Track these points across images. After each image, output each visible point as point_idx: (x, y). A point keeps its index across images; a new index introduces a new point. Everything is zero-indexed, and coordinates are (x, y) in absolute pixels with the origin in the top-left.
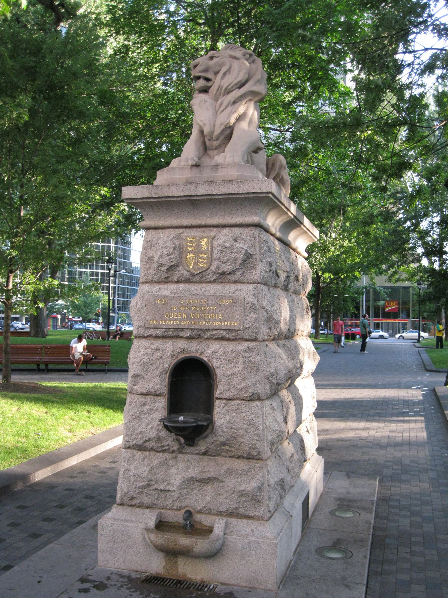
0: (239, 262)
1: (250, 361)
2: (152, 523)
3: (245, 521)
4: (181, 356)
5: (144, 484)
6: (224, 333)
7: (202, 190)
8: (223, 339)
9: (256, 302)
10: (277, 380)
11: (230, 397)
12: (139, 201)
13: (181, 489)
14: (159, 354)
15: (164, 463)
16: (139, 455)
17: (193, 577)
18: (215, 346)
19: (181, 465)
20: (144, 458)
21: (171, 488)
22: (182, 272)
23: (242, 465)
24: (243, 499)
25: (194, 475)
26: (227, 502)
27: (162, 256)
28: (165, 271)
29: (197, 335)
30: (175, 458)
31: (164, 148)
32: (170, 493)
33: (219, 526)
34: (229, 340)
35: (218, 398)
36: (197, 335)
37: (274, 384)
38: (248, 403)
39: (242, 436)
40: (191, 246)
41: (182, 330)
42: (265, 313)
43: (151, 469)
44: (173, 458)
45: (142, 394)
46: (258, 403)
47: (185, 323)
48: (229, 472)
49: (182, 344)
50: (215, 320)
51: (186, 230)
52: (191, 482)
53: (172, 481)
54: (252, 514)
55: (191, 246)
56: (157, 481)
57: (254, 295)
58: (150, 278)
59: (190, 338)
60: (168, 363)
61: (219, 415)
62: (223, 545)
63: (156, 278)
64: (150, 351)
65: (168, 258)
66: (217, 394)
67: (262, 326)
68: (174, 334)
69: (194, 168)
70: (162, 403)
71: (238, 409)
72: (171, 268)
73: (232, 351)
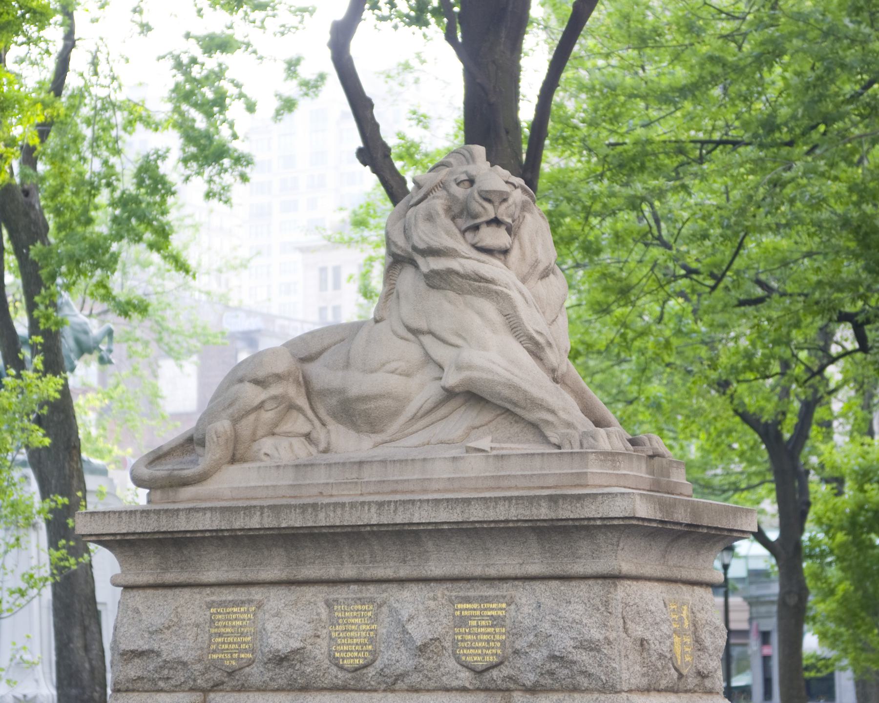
63: (645, 681)
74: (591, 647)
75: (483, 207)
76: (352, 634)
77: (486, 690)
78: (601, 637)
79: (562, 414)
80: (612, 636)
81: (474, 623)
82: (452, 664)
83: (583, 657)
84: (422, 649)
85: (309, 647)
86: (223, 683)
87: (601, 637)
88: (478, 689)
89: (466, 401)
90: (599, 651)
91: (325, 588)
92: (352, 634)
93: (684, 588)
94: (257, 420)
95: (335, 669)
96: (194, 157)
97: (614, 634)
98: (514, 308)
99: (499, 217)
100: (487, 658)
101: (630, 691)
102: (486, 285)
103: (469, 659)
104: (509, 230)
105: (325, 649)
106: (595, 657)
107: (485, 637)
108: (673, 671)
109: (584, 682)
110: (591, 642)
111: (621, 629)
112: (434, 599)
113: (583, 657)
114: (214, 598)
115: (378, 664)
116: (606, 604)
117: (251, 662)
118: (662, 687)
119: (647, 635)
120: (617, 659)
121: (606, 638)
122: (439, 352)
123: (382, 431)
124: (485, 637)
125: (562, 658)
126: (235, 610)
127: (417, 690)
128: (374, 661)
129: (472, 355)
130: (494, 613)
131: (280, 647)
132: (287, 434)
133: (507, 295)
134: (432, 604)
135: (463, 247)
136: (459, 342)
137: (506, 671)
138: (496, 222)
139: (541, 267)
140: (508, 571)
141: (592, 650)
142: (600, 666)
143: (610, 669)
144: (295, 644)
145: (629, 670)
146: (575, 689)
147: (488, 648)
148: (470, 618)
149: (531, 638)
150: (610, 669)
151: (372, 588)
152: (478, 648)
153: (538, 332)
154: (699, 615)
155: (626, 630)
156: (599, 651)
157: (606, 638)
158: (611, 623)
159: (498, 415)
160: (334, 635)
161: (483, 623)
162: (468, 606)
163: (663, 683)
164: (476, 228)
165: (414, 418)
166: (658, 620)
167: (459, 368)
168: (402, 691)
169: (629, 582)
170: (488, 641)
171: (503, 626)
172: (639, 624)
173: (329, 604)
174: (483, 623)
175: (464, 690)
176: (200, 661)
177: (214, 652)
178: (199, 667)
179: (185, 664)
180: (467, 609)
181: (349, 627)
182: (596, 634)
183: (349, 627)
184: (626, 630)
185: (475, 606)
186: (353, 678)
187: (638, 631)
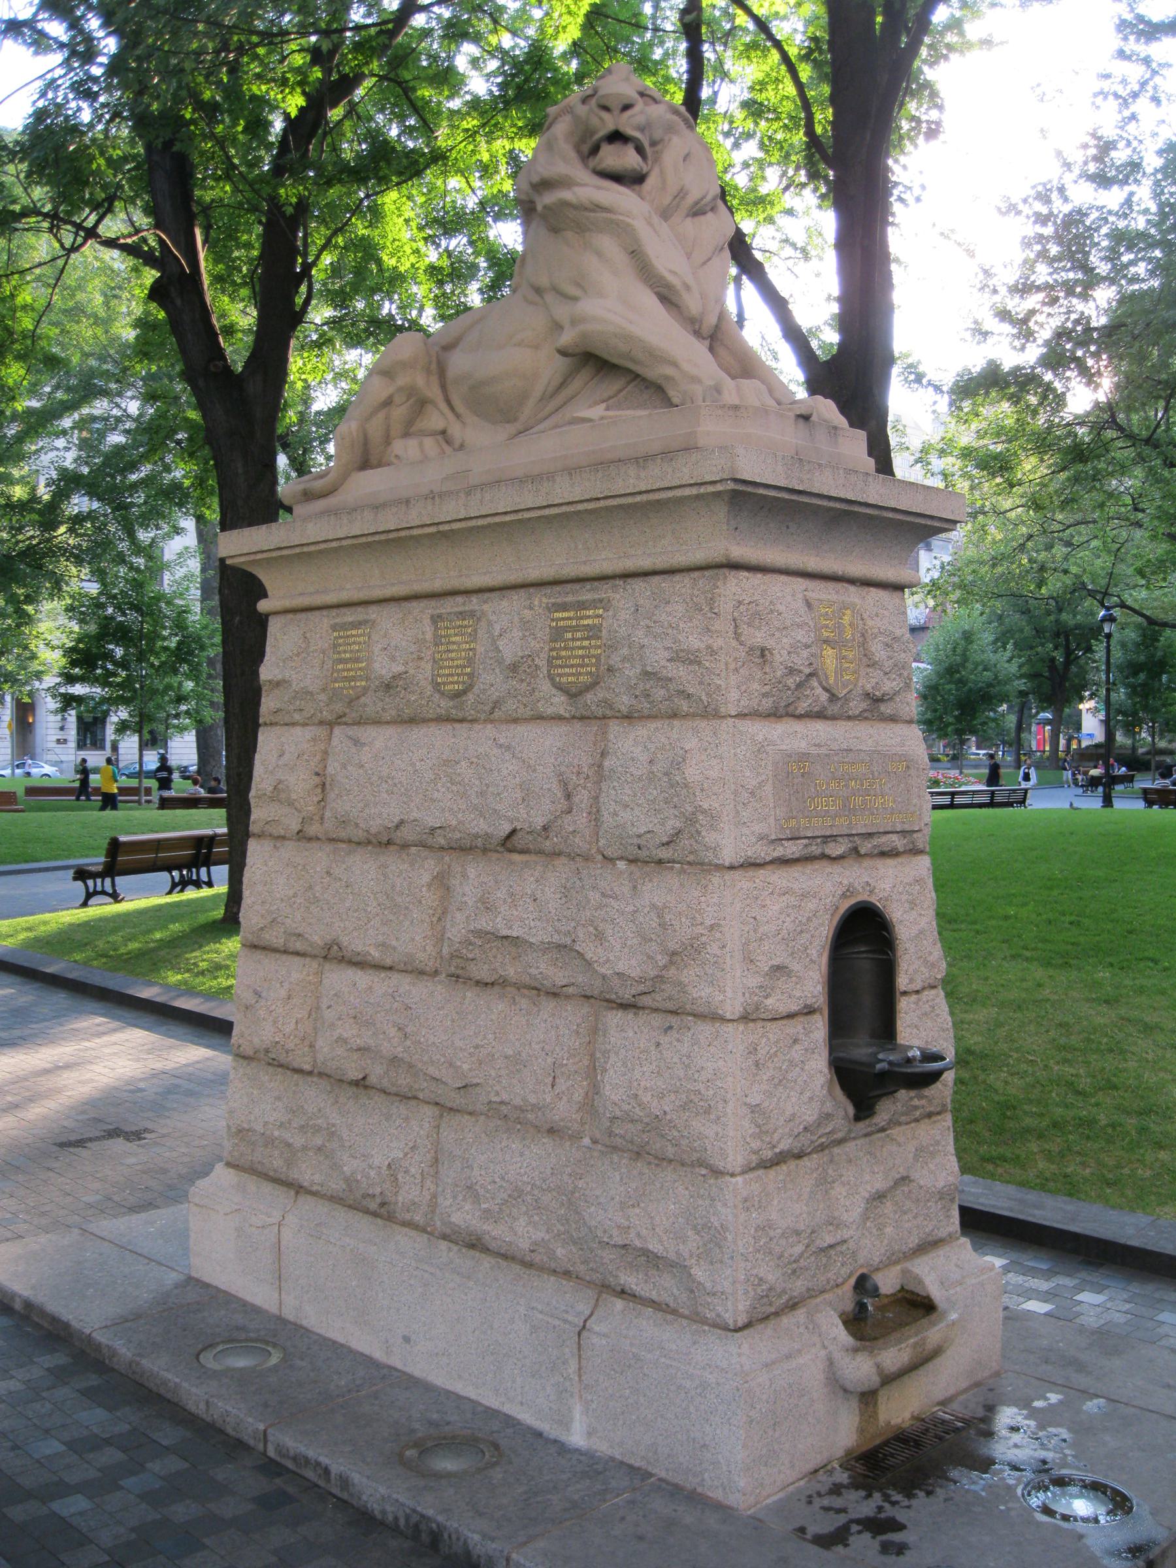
4: (846, 905)
12: (761, 491)
16: (774, 1176)
17: (899, 1420)
21: (846, 1233)
27: (793, 650)
28: (793, 686)
32: (839, 1248)
35: (905, 993)
41: (832, 838)
45: (791, 1016)
47: (841, 825)
53: (845, 1217)
58: (754, 704)
61: (908, 1030)
63: (767, 704)
64: (793, 900)
66: (902, 982)
69: (801, 421)
70: (819, 1029)
74: (690, 659)
75: (601, 119)
76: (453, 655)
77: (582, 718)
78: (703, 646)
79: (685, 366)
80: (718, 643)
81: (569, 635)
82: (545, 687)
83: (680, 672)
84: (514, 668)
85: (412, 671)
86: (345, 715)
87: (703, 646)
88: (574, 717)
89: (598, 371)
90: (699, 663)
91: (433, 603)
92: (453, 655)
93: (852, 588)
94: (387, 418)
95: (437, 696)
96: (1159, 518)
97: (720, 642)
98: (636, 240)
99: (622, 129)
100: (581, 679)
101: (741, 716)
102: (609, 215)
103: (564, 680)
104: (640, 150)
105: (429, 674)
106: (695, 672)
107: (580, 652)
108: (819, 691)
109: (685, 706)
110: (688, 652)
111: (731, 634)
112: (531, 608)
113: (680, 672)
114: (338, 620)
115: (476, 690)
116: (711, 601)
117: (365, 690)
118: (800, 711)
119: (770, 643)
120: (723, 674)
121: (709, 647)
122: (562, 312)
123: (516, 420)
124: (580, 652)
125: (654, 674)
126: (354, 632)
127: (515, 721)
128: (471, 686)
129: (590, 307)
130: (589, 621)
131: (384, 672)
132: (423, 433)
133: (628, 225)
134: (527, 613)
135: (580, 173)
136: (572, 290)
137: (601, 694)
138: (616, 137)
139: (690, 200)
140: (608, 568)
141: (691, 662)
142: (701, 683)
143: (713, 688)
144: (398, 668)
145: (736, 688)
146: (674, 715)
147: (582, 666)
148: (566, 629)
149: (625, 651)
150: (713, 688)
151: (474, 599)
152: (572, 666)
153: (671, 271)
154: (870, 623)
155: (737, 636)
156: (699, 663)
157: (709, 647)
158: (717, 627)
159: (629, 383)
160: (437, 656)
161: (579, 635)
162: (565, 615)
163: (803, 706)
164: (595, 150)
165: (545, 398)
166: (788, 623)
167: (574, 322)
168: (501, 721)
169: (746, 574)
170: (582, 657)
171: (599, 638)
172: (759, 628)
173: (436, 619)
174: (579, 635)
175: (559, 718)
176: (323, 690)
177: (336, 681)
178: (323, 697)
179: (311, 693)
180: (563, 619)
181: (451, 647)
182: (695, 642)
183: (451, 647)
184: (737, 636)
185: (572, 614)
186: (455, 707)
187: (758, 637)
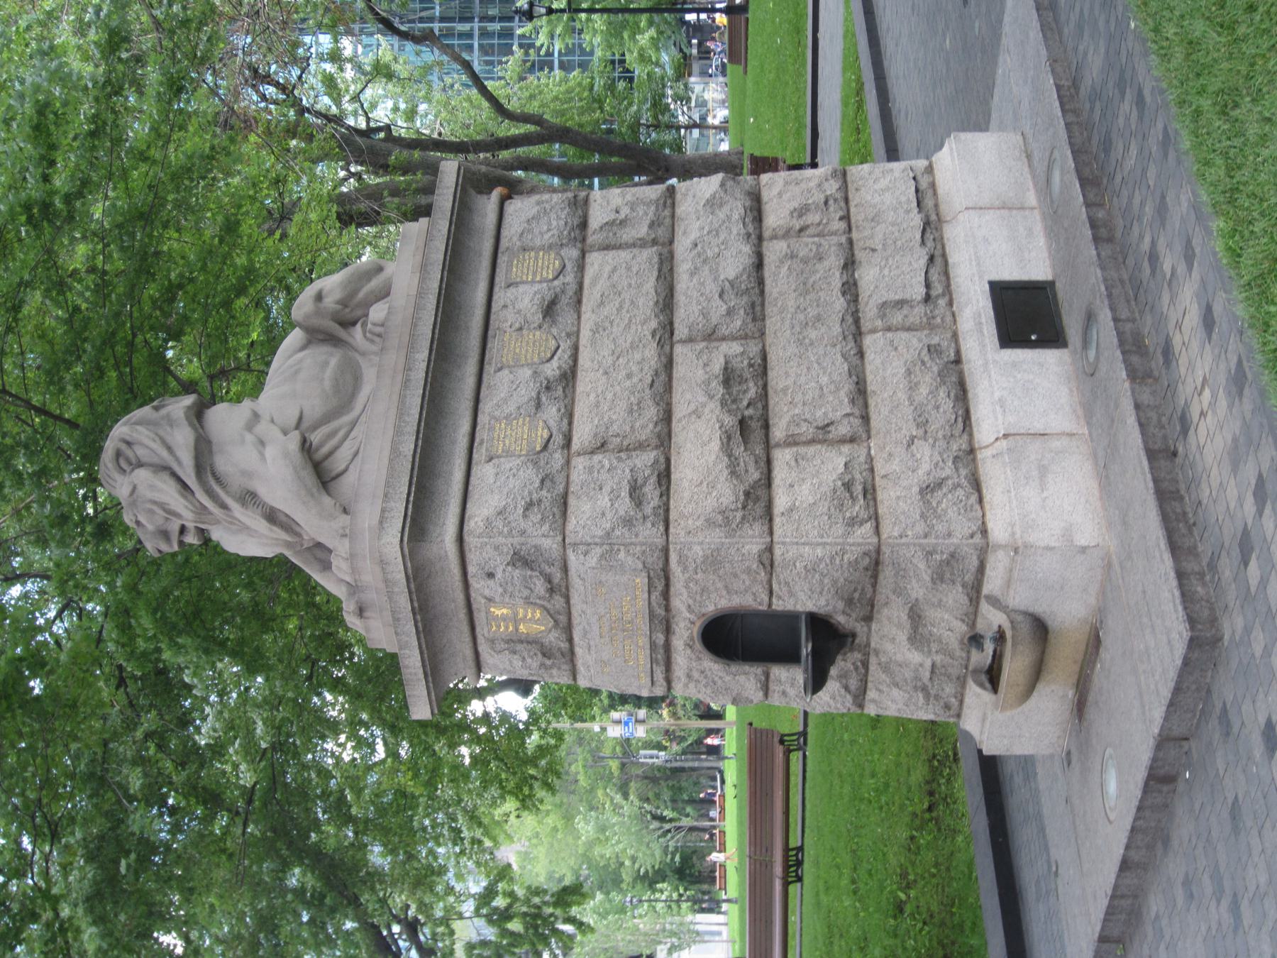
0: (529, 573)
1: (703, 562)
2: (987, 696)
3: (988, 572)
4: (699, 646)
5: (921, 695)
6: (656, 595)
7: (404, 602)
8: (666, 594)
9: (598, 550)
10: (736, 510)
11: (767, 593)
13: (930, 651)
14: (696, 675)
15: (886, 668)
18: (679, 602)
19: (889, 647)
20: (878, 689)
22: (554, 638)
23: (887, 575)
24: (948, 575)
25: (905, 638)
26: (955, 596)
29: (664, 623)
30: (877, 653)
31: (349, 925)
33: (991, 619)
34: (667, 586)
36: (664, 623)
37: (743, 518)
38: (778, 569)
39: (835, 582)
40: (507, 628)
42: (618, 533)
43: (897, 685)
44: (877, 655)
46: (778, 551)
47: (643, 641)
48: (899, 591)
49: (678, 643)
50: (634, 597)
51: (478, 630)
52: (918, 638)
54: (975, 563)
55: (507, 628)
56: (917, 678)
57: (586, 554)
59: (668, 631)
60: (712, 666)
62: (1026, 614)
65: (529, 660)
67: (641, 538)
68: (662, 651)
71: (787, 584)
72: (546, 653)
73: (687, 587)
